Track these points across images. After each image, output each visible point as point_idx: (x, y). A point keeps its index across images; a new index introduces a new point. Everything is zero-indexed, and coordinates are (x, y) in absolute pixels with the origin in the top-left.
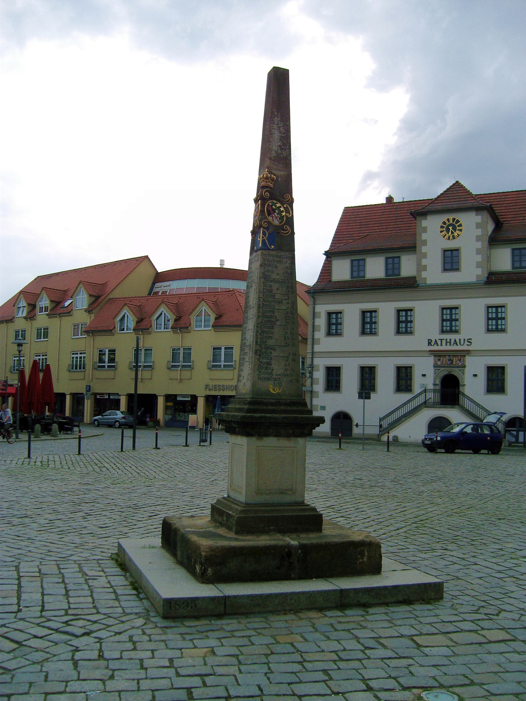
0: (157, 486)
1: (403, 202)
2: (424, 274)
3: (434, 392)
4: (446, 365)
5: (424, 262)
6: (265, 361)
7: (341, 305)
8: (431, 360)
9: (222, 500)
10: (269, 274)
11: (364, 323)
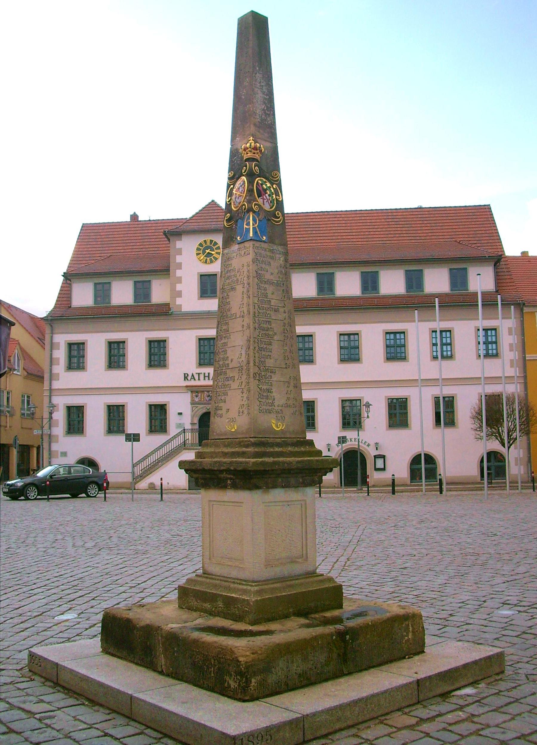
0: (83, 567)
1: (150, 220)
2: (179, 301)
3: (192, 432)
4: (205, 402)
5: (179, 287)
6: (265, 387)
7: (81, 335)
8: (187, 397)
9: (196, 578)
10: (263, 272)
11: (151, 354)
